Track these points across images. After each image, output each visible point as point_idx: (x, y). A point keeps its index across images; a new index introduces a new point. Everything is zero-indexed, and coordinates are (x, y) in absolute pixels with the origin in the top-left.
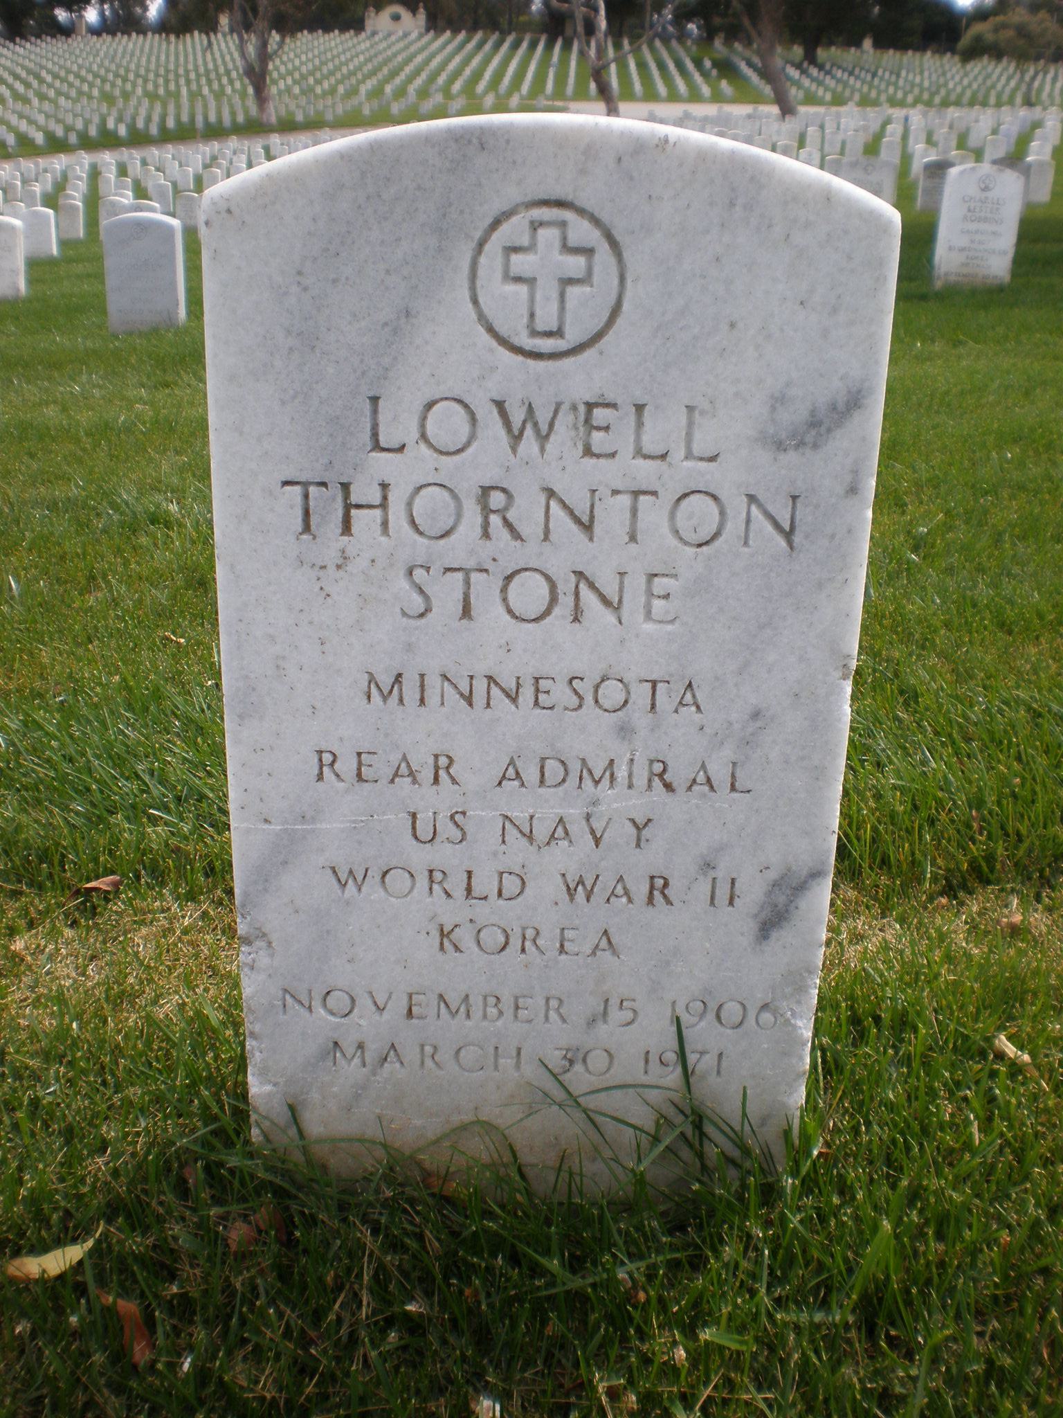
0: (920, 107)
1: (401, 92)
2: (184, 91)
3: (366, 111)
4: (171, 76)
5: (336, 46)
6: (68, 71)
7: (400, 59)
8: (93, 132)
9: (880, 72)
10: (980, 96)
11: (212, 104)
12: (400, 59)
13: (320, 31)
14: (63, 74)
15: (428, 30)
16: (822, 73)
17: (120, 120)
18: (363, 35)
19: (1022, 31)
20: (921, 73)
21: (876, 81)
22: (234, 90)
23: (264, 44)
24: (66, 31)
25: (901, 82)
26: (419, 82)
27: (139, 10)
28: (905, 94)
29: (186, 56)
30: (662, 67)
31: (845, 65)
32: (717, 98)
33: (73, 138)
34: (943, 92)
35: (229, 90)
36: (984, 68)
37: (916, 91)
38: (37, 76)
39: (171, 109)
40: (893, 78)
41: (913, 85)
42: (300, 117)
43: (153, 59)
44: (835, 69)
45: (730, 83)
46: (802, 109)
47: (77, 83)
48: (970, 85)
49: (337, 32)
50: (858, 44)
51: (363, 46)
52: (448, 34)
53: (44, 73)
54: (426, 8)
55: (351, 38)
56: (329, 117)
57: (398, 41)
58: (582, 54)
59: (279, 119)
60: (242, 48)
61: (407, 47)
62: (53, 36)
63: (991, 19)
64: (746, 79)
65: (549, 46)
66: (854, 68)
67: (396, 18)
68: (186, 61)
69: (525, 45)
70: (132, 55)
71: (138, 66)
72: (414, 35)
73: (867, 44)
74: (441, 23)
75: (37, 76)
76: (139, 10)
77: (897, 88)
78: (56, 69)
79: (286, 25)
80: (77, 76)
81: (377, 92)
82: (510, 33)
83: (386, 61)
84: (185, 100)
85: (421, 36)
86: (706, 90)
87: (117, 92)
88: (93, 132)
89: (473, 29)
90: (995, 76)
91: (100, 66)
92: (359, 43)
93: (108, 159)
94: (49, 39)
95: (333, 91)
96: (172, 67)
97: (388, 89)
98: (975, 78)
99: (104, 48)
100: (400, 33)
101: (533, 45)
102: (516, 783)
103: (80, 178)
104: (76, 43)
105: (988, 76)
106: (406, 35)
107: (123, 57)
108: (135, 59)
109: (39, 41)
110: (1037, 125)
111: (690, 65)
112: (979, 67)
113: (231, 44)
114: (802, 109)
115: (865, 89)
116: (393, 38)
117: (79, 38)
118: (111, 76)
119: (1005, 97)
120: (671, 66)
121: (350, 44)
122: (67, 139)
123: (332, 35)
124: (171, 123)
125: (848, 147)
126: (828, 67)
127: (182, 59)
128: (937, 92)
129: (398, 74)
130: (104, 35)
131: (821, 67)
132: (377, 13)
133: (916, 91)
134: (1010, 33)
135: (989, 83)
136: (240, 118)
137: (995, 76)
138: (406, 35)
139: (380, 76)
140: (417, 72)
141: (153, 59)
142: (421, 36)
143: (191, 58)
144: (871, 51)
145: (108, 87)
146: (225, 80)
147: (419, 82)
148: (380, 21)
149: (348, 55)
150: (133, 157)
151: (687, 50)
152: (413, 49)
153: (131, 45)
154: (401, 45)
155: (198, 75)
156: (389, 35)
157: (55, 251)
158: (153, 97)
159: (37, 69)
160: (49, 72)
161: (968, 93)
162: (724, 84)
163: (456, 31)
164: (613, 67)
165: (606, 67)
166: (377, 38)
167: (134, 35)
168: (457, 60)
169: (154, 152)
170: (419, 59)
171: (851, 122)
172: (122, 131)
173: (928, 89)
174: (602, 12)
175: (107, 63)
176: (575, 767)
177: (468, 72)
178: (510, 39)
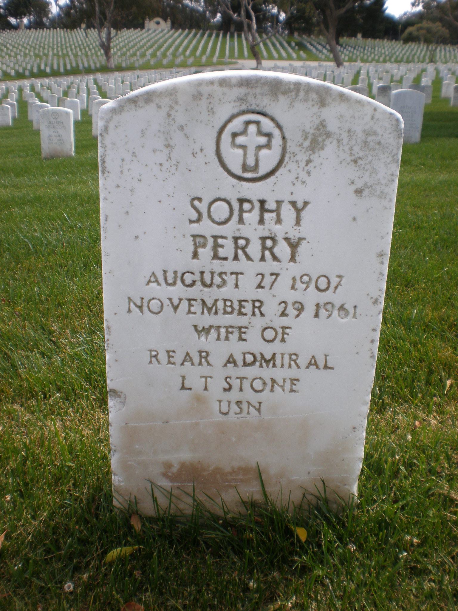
0: (374, 63)
1: (164, 55)
2: (51, 53)
3: (152, 63)
4: (64, 47)
5: (133, 35)
6: (19, 45)
7: (161, 41)
8: (35, 70)
9: (367, 48)
10: (410, 59)
11: (85, 60)
12: (161, 41)
13: (125, 29)
14: (16, 45)
15: (172, 29)
16: (342, 49)
17: (46, 65)
18: (144, 30)
19: (429, 30)
20: (384, 48)
21: (366, 52)
22: (82, 54)
23: (109, 34)
24: (15, 28)
25: (376, 52)
26: (171, 50)
27: (38, 20)
28: (368, 57)
29: (69, 39)
30: (274, 45)
31: (351, 45)
32: (299, 58)
33: (27, 73)
34: (395, 56)
35: (80, 53)
36: (410, 46)
37: (373, 55)
38: (5, 46)
39: (67, 61)
40: (373, 50)
41: (381, 54)
42: (124, 65)
43: (55, 39)
44: (347, 46)
45: (304, 52)
46: (346, 64)
47: (23, 49)
48: (385, 53)
49: (132, 29)
50: (355, 36)
51: (145, 35)
52: (180, 30)
53: (8, 45)
54: (170, 19)
55: (139, 32)
56: (137, 65)
57: (159, 33)
58: (247, 39)
59: (115, 66)
60: (99, 35)
61: (164, 36)
62: (10, 30)
63: (416, 25)
64: (310, 51)
65: (225, 36)
66: (355, 46)
67: (158, 23)
68: (69, 41)
69: (214, 35)
70: (45, 38)
71: (49, 43)
72: (166, 31)
73: (359, 36)
74: (176, 26)
75: (5, 46)
76: (38, 20)
77: (364, 54)
78: (13, 43)
79: (118, 26)
80: (23, 46)
81: (154, 55)
82: (207, 30)
83: (156, 42)
84: (72, 57)
85: (169, 31)
86: (294, 55)
87: (41, 54)
88: (35, 70)
89: (190, 28)
90: (396, 49)
91: (33, 42)
92: (143, 34)
93: (26, 83)
94: (8, 30)
95: (135, 54)
96: (63, 43)
97: (158, 53)
98: (407, 51)
99: (33, 34)
100: (160, 30)
101: (217, 36)
102: (233, 365)
103: (14, 92)
104: (20, 32)
105: (394, 49)
106: (162, 31)
107: (42, 38)
108: (47, 40)
109: (4, 32)
110: (424, 70)
111: (286, 45)
112: (413, 46)
113: (95, 33)
114: (346, 64)
115: (351, 55)
116: (157, 32)
117: (21, 30)
118: (29, 47)
119: (410, 59)
120: (278, 45)
121: (139, 34)
122: (24, 73)
123: (131, 30)
124: (68, 67)
125: (345, 80)
126: (344, 46)
127: (67, 40)
128: (381, 56)
129: (179, 48)
130: (32, 29)
131: (341, 46)
132: (150, 21)
133: (373, 55)
134: (423, 32)
135: (393, 52)
136: (98, 65)
137: (415, 50)
138: (162, 31)
139: (154, 48)
140: (170, 47)
141: (55, 39)
142: (169, 31)
143: (71, 39)
144: (361, 39)
145: (37, 52)
146: (69, 49)
147: (171, 50)
148: (150, 24)
149: (139, 39)
150: (38, 82)
151: (284, 38)
152: (166, 37)
153: (44, 34)
154: (161, 35)
155: (76, 47)
156: (155, 31)
157: (10, 123)
158: (36, 55)
159: (5, 43)
160: (10, 45)
161: (405, 57)
162: (302, 52)
163: (184, 29)
164: (261, 45)
165: (258, 44)
166: (150, 32)
167: (45, 29)
168: (186, 41)
169: (46, 81)
170: (170, 41)
171: (368, 69)
172: (48, 70)
173: (388, 55)
174: (254, 21)
175: (35, 41)
176: (259, 357)
177: (191, 46)
178: (207, 33)
